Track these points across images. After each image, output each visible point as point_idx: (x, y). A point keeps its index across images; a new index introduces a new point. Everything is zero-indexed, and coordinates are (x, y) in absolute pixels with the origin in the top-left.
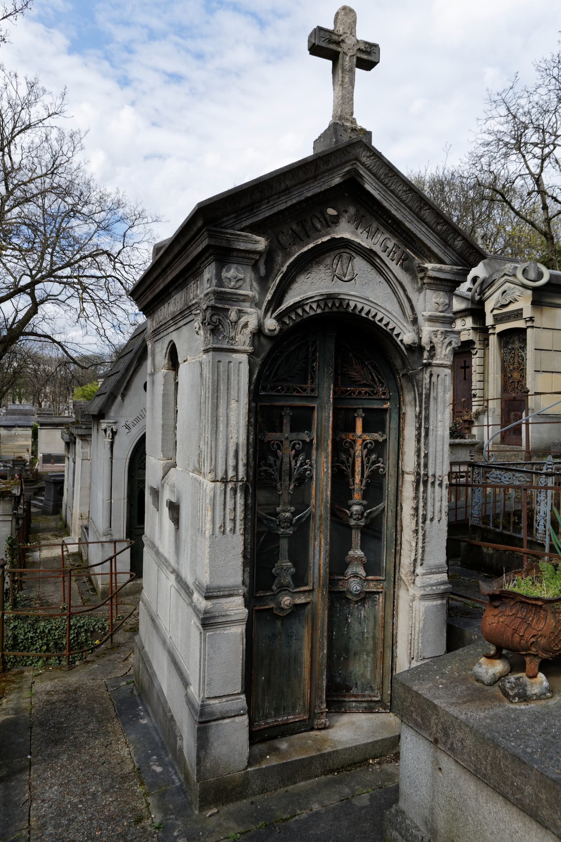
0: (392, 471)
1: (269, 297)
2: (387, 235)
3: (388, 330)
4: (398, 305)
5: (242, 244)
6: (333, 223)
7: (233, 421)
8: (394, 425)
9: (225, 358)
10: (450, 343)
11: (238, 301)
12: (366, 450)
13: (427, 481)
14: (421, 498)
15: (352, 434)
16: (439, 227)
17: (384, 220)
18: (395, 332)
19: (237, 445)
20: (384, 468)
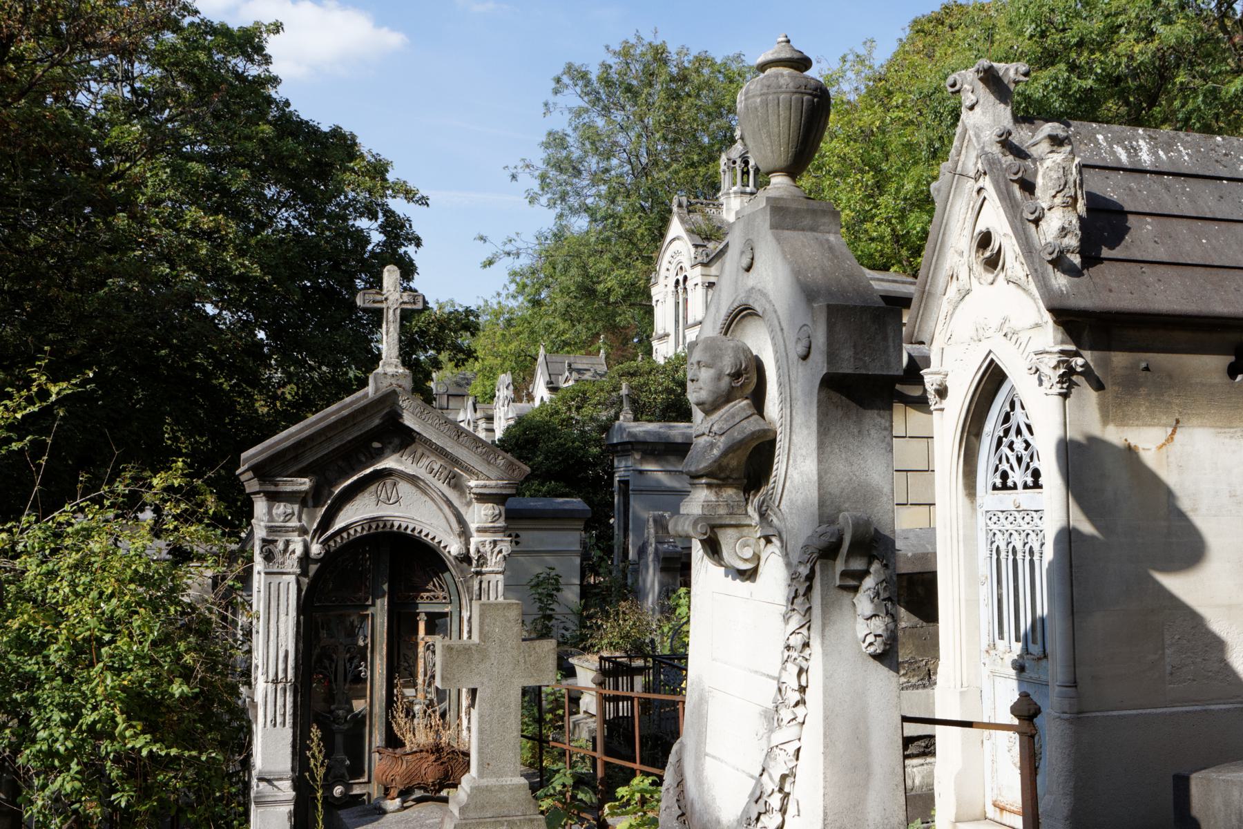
1: (315, 526)
2: (433, 458)
7: (282, 632)
8: (455, 627)
9: (275, 580)
10: (500, 552)
19: (287, 652)
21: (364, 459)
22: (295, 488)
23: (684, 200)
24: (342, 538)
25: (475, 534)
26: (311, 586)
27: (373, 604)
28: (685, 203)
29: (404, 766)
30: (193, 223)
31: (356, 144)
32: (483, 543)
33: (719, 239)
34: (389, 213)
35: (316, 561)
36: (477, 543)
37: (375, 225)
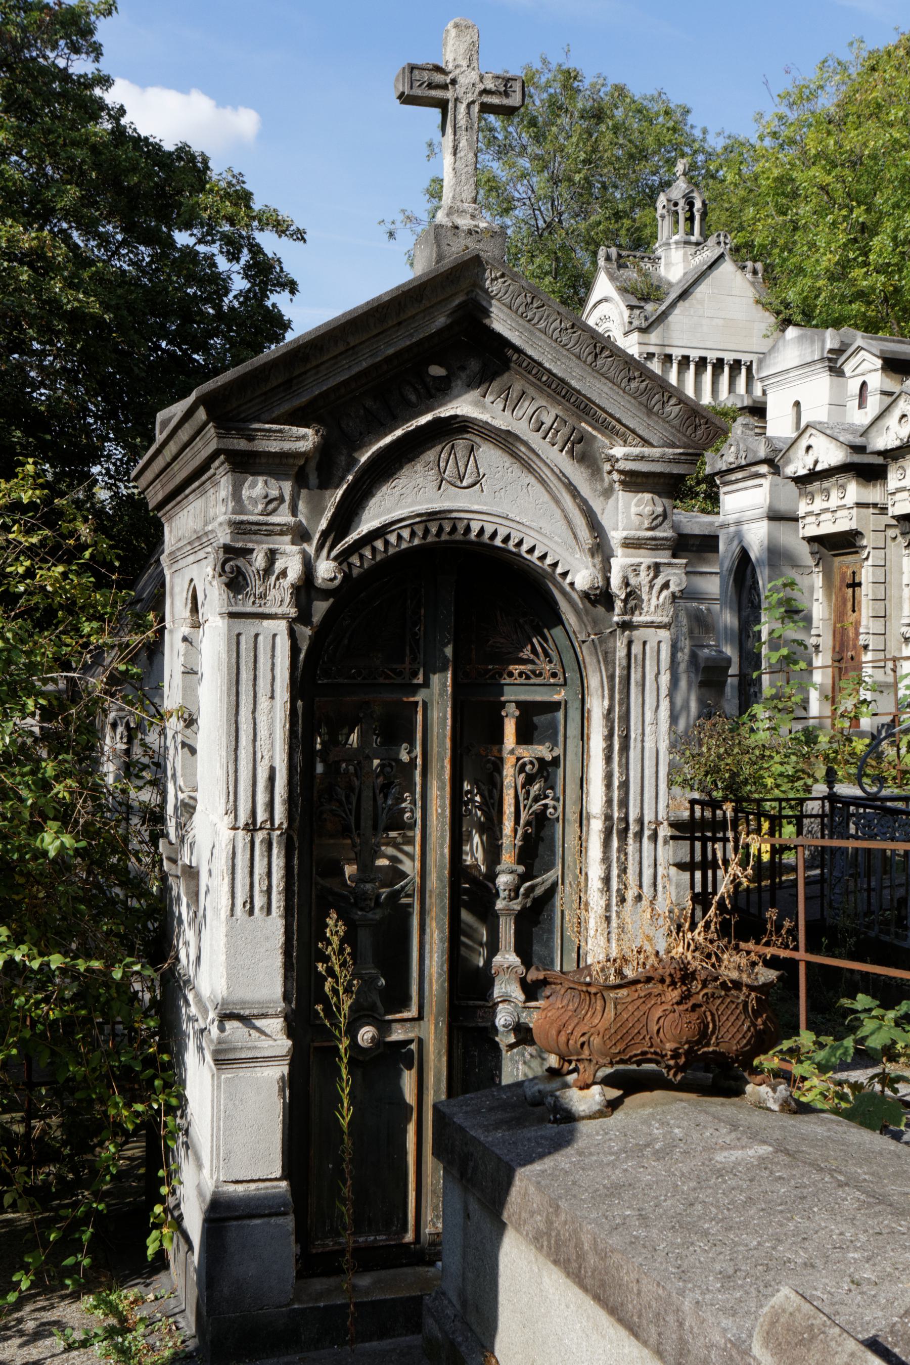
0: (572, 815)
1: (323, 524)
3: (546, 567)
4: (563, 522)
5: (274, 443)
6: (439, 390)
7: (263, 732)
8: (573, 730)
9: (249, 628)
10: (666, 586)
11: (270, 534)
12: (523, 775)
13: (626, 829)
14: (615, 860)
15: (497, 747)
16: (634, 385)
17: (535, 376)
18: (559, 570)
19: (272, 770)
20: (555, 808)
21: (413, 398)
22: (287, 446)
23: (613, 251)
24: (374, 550)
25: (619, 551)
26: (316, 641)
27: (426, 684)
28: (614, 256)
29: (610, 1013)
30: (8, 240)
31: (208, 168)
32: (636, 568)
33: (659, 300)
34: (256, 250)
35: (325, 594)
36: (624, 568)
37: (236, 267)
